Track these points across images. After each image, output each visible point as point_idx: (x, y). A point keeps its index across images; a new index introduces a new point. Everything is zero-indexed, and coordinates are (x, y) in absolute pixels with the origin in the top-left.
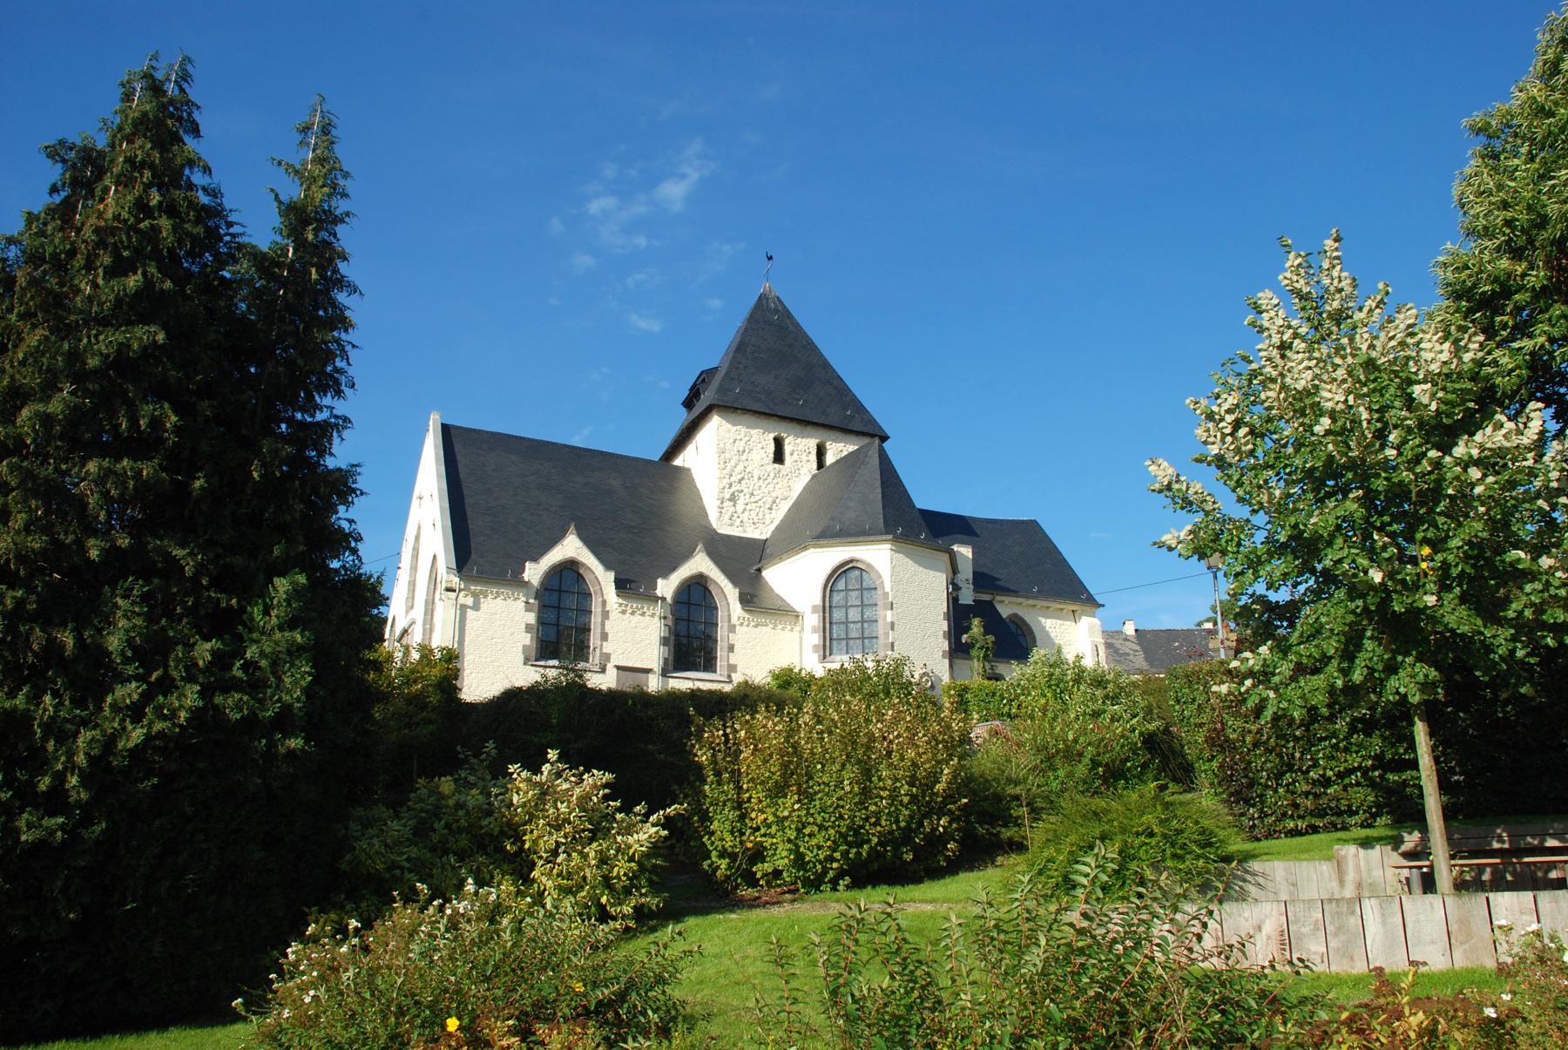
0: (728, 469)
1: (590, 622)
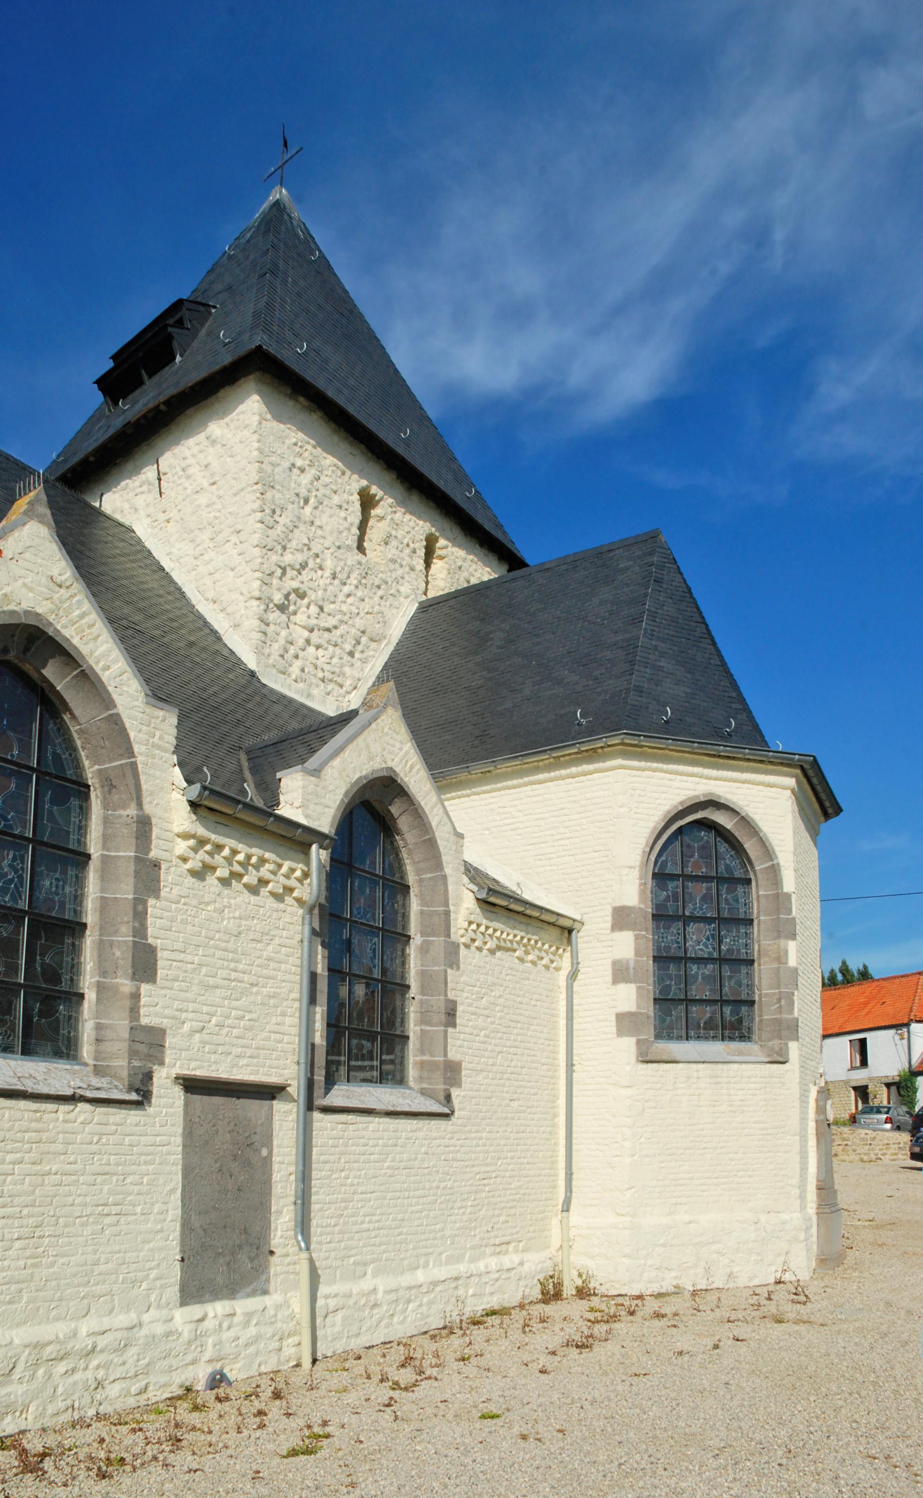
1: (78, 898)
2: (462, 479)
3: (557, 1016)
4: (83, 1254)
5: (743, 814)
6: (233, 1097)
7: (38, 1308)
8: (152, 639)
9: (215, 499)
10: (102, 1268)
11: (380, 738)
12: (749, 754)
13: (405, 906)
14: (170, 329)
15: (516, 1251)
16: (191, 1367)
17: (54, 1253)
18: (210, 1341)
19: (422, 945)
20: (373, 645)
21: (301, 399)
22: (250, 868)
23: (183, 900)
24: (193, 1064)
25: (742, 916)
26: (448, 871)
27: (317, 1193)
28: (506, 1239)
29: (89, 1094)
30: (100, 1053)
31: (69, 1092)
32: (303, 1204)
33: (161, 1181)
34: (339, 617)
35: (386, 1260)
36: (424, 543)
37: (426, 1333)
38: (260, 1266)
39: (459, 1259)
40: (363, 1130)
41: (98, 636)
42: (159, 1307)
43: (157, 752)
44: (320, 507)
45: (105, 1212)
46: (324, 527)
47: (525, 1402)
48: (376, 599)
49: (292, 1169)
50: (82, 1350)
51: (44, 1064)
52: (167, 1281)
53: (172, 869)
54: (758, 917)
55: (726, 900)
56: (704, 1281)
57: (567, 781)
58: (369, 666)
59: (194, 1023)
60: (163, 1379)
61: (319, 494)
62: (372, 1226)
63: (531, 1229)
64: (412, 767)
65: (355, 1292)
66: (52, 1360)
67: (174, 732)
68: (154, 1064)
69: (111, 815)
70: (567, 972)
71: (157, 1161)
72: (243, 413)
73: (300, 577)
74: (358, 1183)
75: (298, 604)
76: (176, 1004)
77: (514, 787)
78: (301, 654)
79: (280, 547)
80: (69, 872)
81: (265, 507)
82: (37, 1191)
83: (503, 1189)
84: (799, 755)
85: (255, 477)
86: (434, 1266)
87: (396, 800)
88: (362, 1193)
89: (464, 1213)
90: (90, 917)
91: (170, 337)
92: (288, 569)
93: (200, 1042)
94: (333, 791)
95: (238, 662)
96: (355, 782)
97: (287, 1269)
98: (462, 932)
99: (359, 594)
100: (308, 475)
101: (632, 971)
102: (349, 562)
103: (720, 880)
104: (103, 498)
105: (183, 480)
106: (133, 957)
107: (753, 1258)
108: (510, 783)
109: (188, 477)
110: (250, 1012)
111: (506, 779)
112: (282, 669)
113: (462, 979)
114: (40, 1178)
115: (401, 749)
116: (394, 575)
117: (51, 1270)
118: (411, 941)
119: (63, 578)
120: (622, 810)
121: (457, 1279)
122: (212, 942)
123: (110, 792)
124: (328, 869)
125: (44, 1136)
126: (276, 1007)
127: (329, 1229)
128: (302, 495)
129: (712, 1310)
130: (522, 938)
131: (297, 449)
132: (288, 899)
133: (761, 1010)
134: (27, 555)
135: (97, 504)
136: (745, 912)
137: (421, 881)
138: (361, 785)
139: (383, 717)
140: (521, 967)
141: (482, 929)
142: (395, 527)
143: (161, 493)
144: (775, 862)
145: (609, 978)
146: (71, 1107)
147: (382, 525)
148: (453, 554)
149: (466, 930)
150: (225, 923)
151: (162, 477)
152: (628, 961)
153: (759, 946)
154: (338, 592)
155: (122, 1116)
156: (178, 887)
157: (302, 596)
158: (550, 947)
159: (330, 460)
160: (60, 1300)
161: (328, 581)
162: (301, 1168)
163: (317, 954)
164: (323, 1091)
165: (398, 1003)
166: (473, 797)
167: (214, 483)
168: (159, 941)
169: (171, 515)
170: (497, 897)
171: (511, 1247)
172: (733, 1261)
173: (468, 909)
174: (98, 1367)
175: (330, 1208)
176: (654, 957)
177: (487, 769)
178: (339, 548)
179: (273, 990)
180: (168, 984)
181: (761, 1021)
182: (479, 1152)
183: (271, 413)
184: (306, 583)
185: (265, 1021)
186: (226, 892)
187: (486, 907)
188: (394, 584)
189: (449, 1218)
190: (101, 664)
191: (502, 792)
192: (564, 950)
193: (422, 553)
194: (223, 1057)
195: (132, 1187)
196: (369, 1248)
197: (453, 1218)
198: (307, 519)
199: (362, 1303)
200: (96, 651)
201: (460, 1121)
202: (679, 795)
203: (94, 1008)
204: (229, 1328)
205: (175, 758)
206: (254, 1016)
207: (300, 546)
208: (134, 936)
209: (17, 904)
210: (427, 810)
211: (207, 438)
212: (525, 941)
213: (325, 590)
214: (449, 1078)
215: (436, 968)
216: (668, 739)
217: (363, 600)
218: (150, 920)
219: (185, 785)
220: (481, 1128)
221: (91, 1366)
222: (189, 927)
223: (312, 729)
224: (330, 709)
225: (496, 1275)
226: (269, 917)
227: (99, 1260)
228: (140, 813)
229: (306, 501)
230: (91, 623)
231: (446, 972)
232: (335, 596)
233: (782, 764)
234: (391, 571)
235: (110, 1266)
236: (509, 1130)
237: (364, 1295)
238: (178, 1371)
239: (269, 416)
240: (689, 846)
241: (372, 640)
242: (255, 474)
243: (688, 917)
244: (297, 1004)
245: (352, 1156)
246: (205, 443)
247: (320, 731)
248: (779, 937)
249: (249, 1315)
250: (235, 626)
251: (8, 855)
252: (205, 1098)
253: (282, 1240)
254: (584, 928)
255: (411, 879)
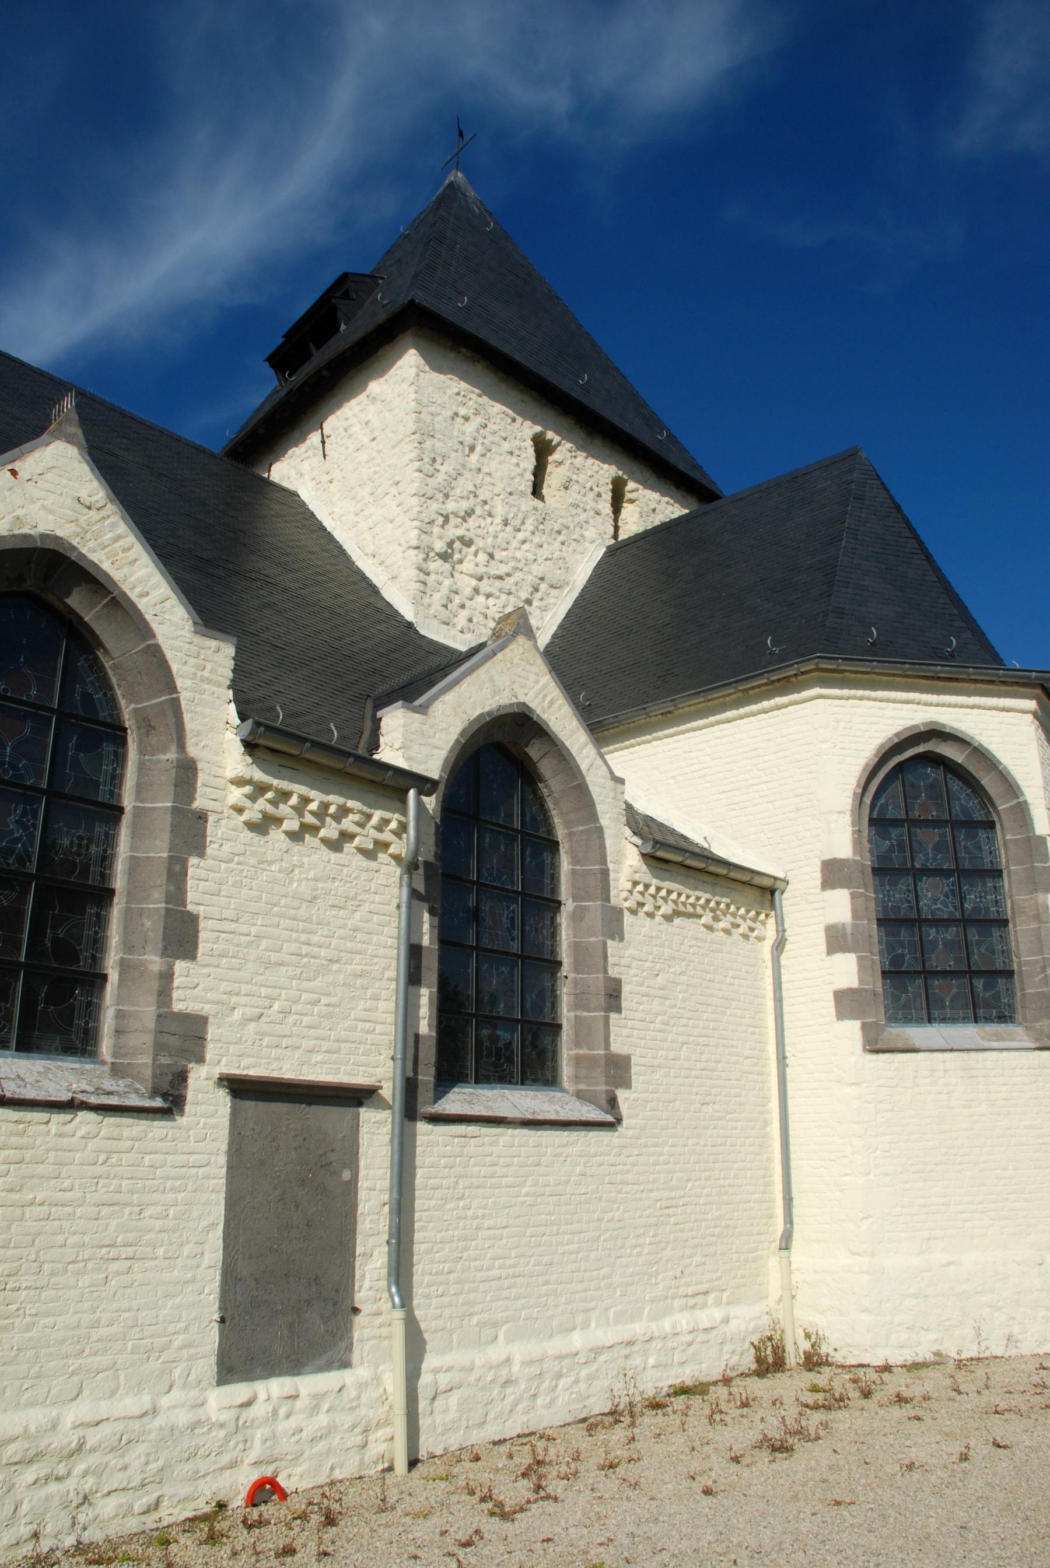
0: (440, 477)
1: (106, 860)
2: (653, 422)
3: (764, 997)
4: (75, 1313)
5: (976, 744)
6: (301, 1103)
7: (5, 1388)
9: (375, 454)
10: (103, 1332)
11: (508, 670)
12: (973, 674)
13: (555, 866)
15: (718, 1303)
16: (228, 1471)
17: (33, 1312)
18: (258, 1435)
19: (574, 911)
20: (554, 592)
21: (464, 350)
22: (328, 819)
23: (236, 858)
24: (245, 1062)
25: (988, 866)
26: (604, 821)
27: (423, 1229)
28: (704, 1287)
29: (93, 1100)
30: (120, 1048)
31: (65, 1097)
32: (399, 1243)
33: (195, 1214)
34: (512, 564)
35: (526, 1319)
36: (611, 487)
37: (584, 1420)
38: (337, 1329)
39: (634, 1316)
40: (491, 1144)
41: (136, 560)
42: (184, 1385)
43: (207, 686)
44: (488, 454)
45: (111, 1255)
47: (659, 1546)
48: (557, 545)
49: (386, 1197)
50: (62, 1449)
51: (43, 1062)
52: (199, 1350)
53: (223, 822)
54: (1007, 867)
55: (965, 847)
56: (975, 1347)
58: (550, 614)
59: (248, 1010)
60: (183, 1491)
61: (485, 441)
62: (504, 1272)
63: (740, 1272)
64: (552, 703)
65: (478, 1363)
66: (16, 1464)
67: (231, 664)
68: (190, 1062)
69: (148, 760)
70: (772, 942)
71: (190, 1187)
72: (401, 367)
74: (484, 1215)
75: (464, 552)
76: (223, 986)
77: (700, 728)
78: (468, 603)
80: (97, 829)
81: (424, 456)
82: (14, 1226)
83: (696, 1221)
84: (1037, 672)
85: (412, 427)
86: (597, 1326)
87: (533, 741)
88: (489, 1229)
89: (639, 1254)
90: (119, 882)
91: (334, 309)
92: (451, 517)
93: (256, 1033)
94: (446, 729)
96: (475, 719)
97: (379, 1332)
98: (625, 894)
99: (536, 540)
101: (849, 937)
102: (523, 508)
103: (955, 824)
105: (346, 440)
106: (165, 928)
107: (1041, 1314)
108: (694, 724)
109: (350, 436)
110: (329, 995)
111: (690, 721)
112: (447, 620)
113: (627, 953)
114: (19, 1210)
115: (537, 682)
116: (576, 520)
117: (27, 1335)
118: (562, 907)
119: (93, 499)
120: (824, 746)
121: (630, 1343)
122: (275, 909)
123: (148, 734)
124: (438, 820)
125: (28, 1155)
126: (365, 988)
127: (440, 1278)
128: (466, 444)
129: (978, 1392)
130: (708, 901)
131: (460, 398)
132: (382, 857)
133: (1022, 982)
134: (49, 476)
135: (266, 475)
136: (991, 862)
137: (570, 835)
138: (483, 722)
140: (709, 936)
141: (652, 890)
143: (324, 456)
144: (1021, 799)
145: (823, 947)
146: (69, 1117)
148: (644, 496)
149: (631, 892)
150: (295, 885)
152: (844, 924)
153: (1012, 902)
154: (511, 539)
155: (142, 1128)
156: (230, 843)
157: (468, 543)
158: (748, 911)
159: (498, 408)
160: (38, 1376)
161: (499, 528)
162: (395, 1196)
163: (422, 922)
164: (431, 1094)
165: (548, 984)
166: (654, 743)
167: (374, 439)
168: (202, 908)
171: (712, 1296)
172: (1014, 1318)
173: (631, 866)
174: (85, 1473)
175: (443, 1249)
176: (878, 920)
178: (511, 494)
179: (360, 967)
180: (214, 961)
181: (1023, 996)
182: (659, 1173)
184: (472, 531)
186: (296, 848)
188: (577, 529)
189: (619, 1261)
190: (137, 591)
191: (687, 735)
192: (767, 916)
193: (608, 496)
194: (288, 1052)
195: (153, 1221)
196: (500, 1303)
197: (624, 1260)
198: (473, 467)
199: (489, 1379)
200: (131, 576)
201: (630, 1132)
202: (893, 725)
203: (116, 992)
204: (288, 1416)
205: (230, 694)
206: (334, 1000)
207: (465, 494)
208: (167, 902)
209: (24, 866)
210: (574, 750)
212: (712, 904)
214: (614, 1077)
215: (593, 939)
216: (873, 661)
217: (541, 546)
218: (190, 883)
219: (238, 722)
220: (660, 1140)
221: (75, 1473)
224: (463, 648)
225: (689, 1338)
226: (356, 878)
227: (99, 1320)
228: (182, 757)
229: (472, 449)
230: (127, 546)
231: (605, 944)
232: (508, 543)
233: (1017, 684)
234: (573, 516)
235: (115, 1329)
236: (702, 1142)
237: (491, 1368)
238: (208, 1479)
239: (427, 368)
240: (913, 785)
241: (552, 587)
243: (919, 869)
244: (393, 986)
245: (474, 1180)
248: (1035, 891)
249: (318, 1398)
251: (15, 811)
252: (262, 1105)
253: (371, 1293)
254: (789, 887)
255: (561, 833)
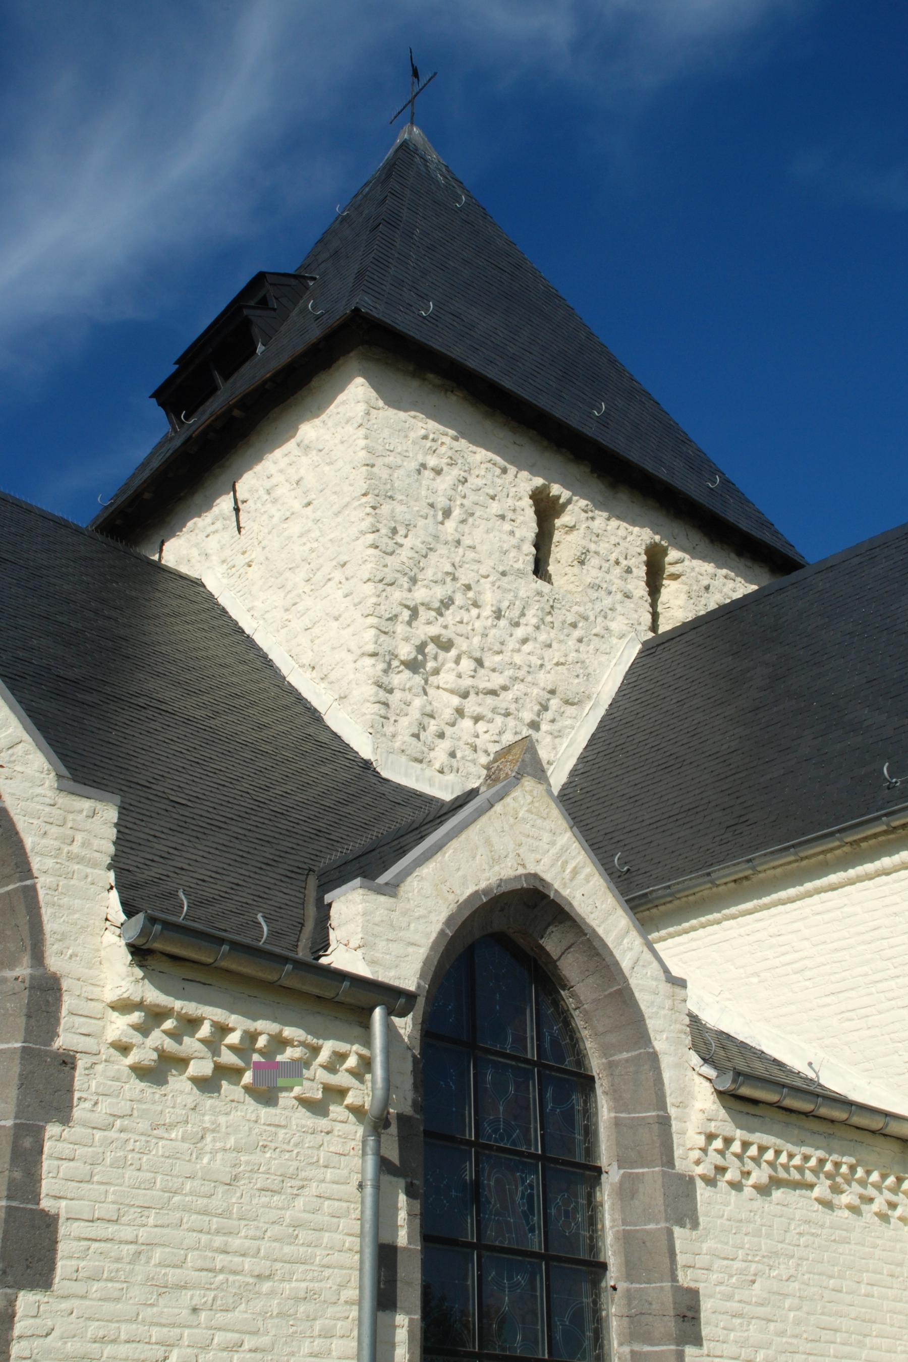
8: (187, 721)
11: (512, 826)
13: (589, 1114)
14: (246, 312)
20: (570, 710)
21: (431, 376)
26: (659, 1044)
34: (510, 672)
36: (644, 558)
43: (76, 867)
44: (470, 520)
46: (478, 548)
48: (571, 643)
53: (99, 1068)
57: (878, 880)
61: (465, 501)
64: (575, 872)
73: (441, 619)
75: (440, 658)
77: (791, 900)
78: (449, 731)
79: (406, 579)
81: (380, 526)
85: (362, 486)
87: (551, 929)
91: (247, 324)
92: (421, 610)
95: (342, 750)
98: (696, 1154)
99: (543, 637)
100: (448, 478)
102: (522, 593)
104: (164, 547)
105: (269, 505)
108: (783, 894)
109: (275, 501)
110: (256, 1333)
113: (705, 1247)
115: (553, 843)
116: (598, 606)
118: (604, 1177)
122: (177, 1199)
124: (417, 1052)
126: (311, 1319)
128: (439, 506)
130: (822, 1162)
131: (428, 444)
132: (337, 1111)
135: (156, 557)
137: (611, 1066)
139: (514, 794)
140: (828, 1217)
141: (736, 1147)
142: (594, 538)
143: (239, 529)
147: (573, 537)
148: (693, 569)
150: (205, 1160)
151: (241, 506)
154: (507, 638)
157: (446, 646)
158: (884, 1177)
159: (482, 454)
161: (489, 622)
163: (396, 1209)
165: (587, 1301)
166: (726, 924)
167: (309, 504)
168: (63, 1203)
169: (253, 556)
170: (756, 1087)
173: (703, 1111)
177: (741, 875)
178: (504, 574)
179: (303, 1285)
180: (79, 1288)
183: (382, 399)
185: (288, 1350)
186: (209, 1102)
187: (739, 1106)
191: (773, 910)
198: (450, 538)
205: (111, 876)
207: (440, 576)
208: (9, 1198)
210: (610, 940)
211: (298, 445)
212: (828, 1167)
213: (485, 635)
215: (652, 1226)
217: (550, 646)
218: (47, 1164)
219: (122, 917)
222: (129, 1173)
223: (414, 826)
228: (39, 972)
229: (447, 513)
231: (670, 1233)
232: (502, 643)
234: (592, 601)
239: (381, 403)
241: (567, 702)
242: (361, 483)
244: (354, 1313)
246: (296, 451)
247: (422, 829)
250: (341, 698)
255: (596, 1064)
